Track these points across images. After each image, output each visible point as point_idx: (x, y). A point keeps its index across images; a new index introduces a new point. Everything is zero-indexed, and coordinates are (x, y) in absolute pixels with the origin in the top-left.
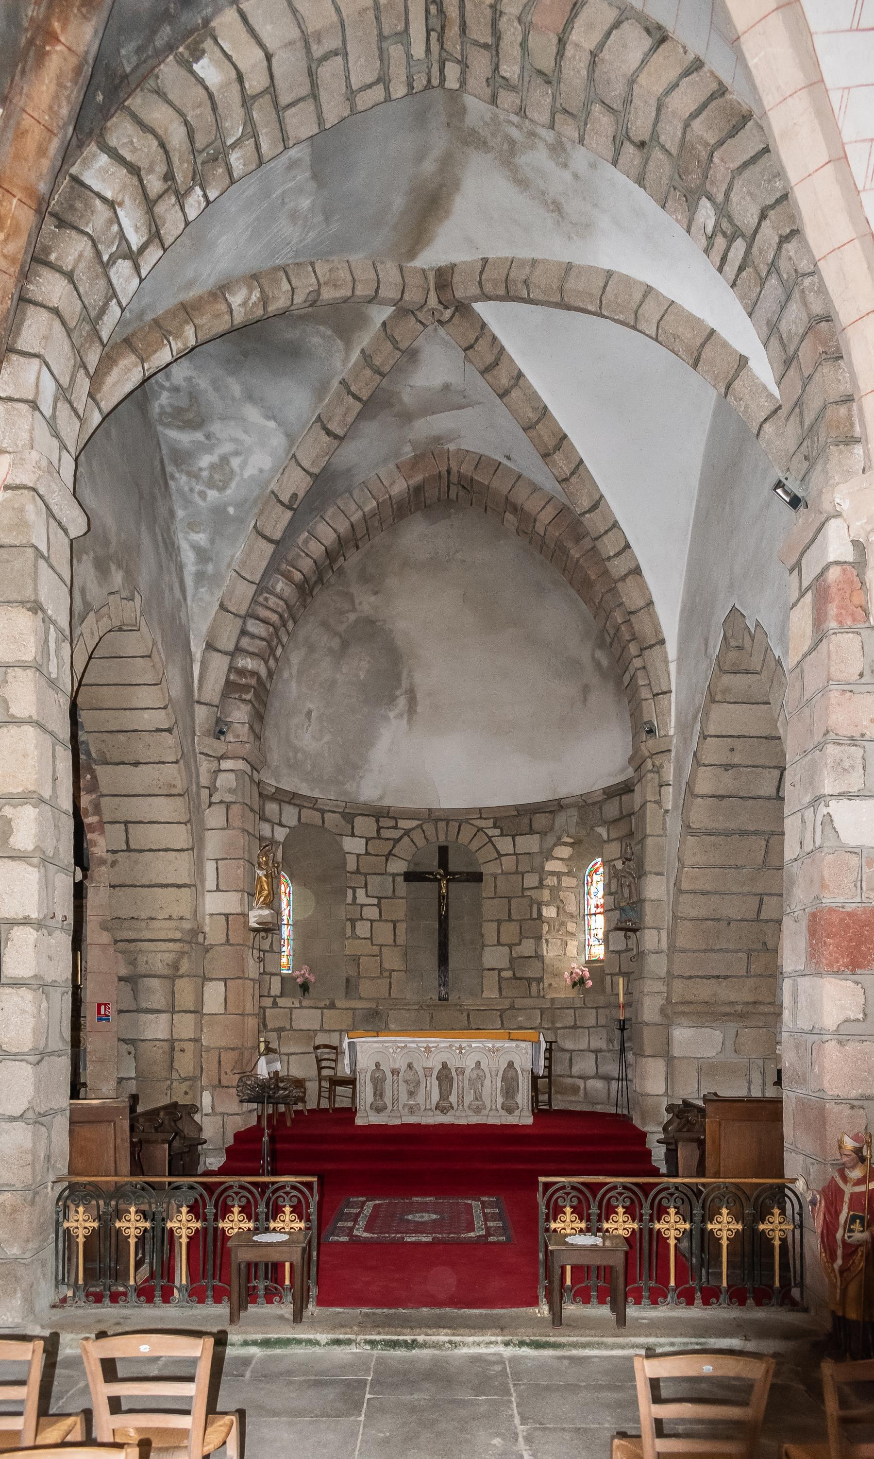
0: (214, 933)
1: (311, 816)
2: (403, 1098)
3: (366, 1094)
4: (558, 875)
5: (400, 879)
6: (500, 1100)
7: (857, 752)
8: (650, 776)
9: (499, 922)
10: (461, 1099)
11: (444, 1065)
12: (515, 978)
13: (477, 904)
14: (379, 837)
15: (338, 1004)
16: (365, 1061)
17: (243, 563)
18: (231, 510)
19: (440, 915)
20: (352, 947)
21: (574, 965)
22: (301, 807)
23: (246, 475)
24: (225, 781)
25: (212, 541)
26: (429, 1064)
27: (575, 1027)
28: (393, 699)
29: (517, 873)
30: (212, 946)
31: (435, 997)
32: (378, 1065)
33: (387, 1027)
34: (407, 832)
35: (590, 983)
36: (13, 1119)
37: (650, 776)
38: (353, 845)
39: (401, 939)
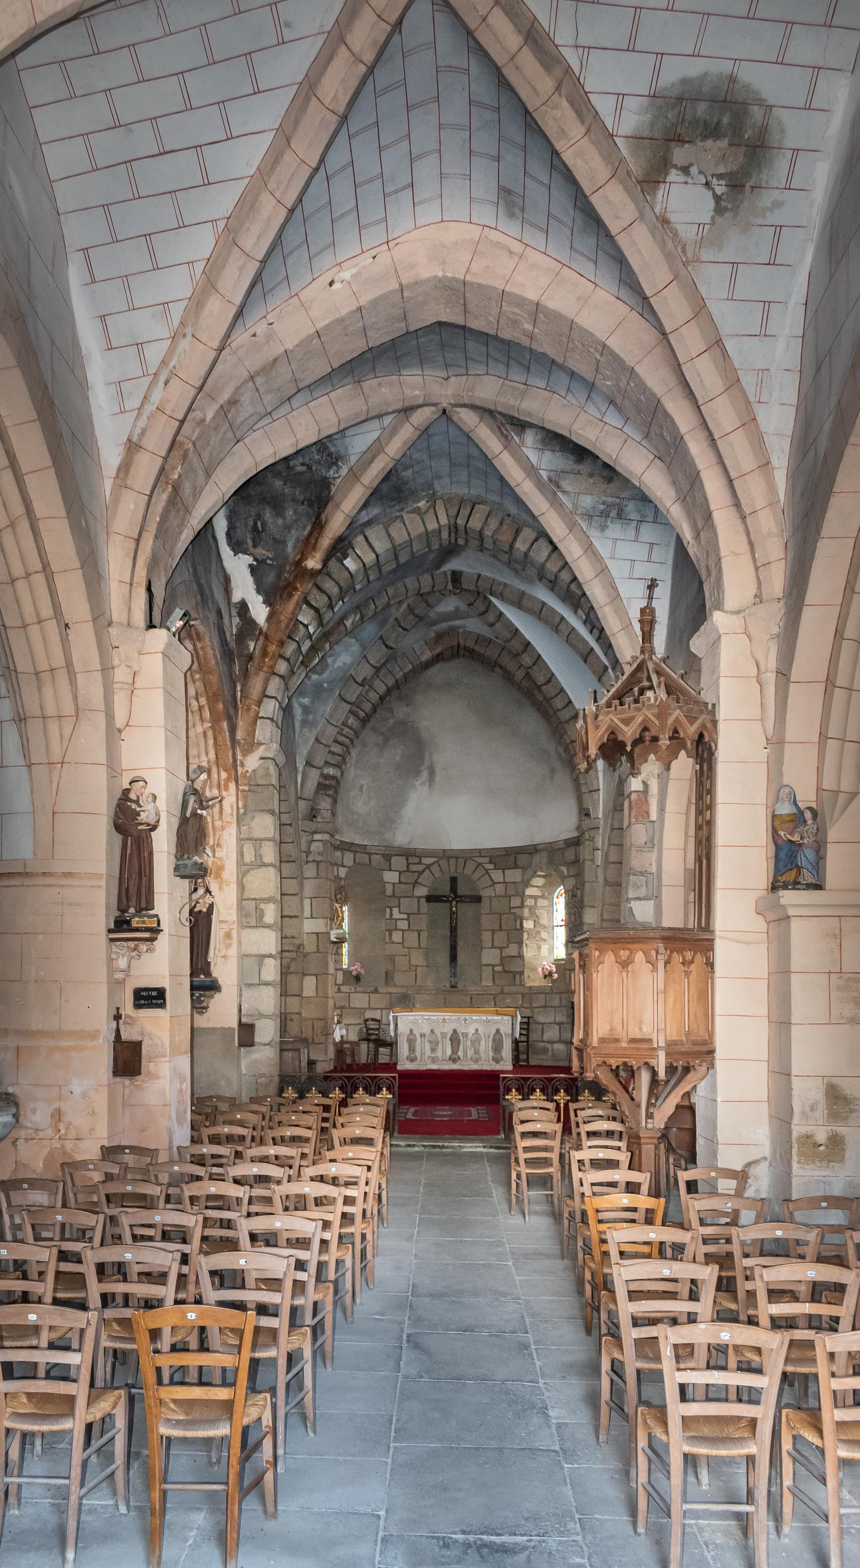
0: (310, 946)
1: (363, 858)
2: (428, 1052)
3: (403, 1050)
4: (535, 898)
5: (423, 900)
6: (491, 1054)
7: (643, 879)
8: (587, 843)
9: (493, 931)
10: (465, 1054)
11: (455, 1031)
12: (505, 971)
13: (478, 919)
14: (408, 870)
15: (381, 990)
16: (403, 1029)
17: (331, 715)
18: (325, 685)
19: (451, 927)
20: (390, 949)
21: (545, 963)
22: (355, 852)
23: (336, 666)
24: (316, 847)
25: (312, 702)
26: (445, 1030)
27: (545, 1007)
28: (418, 773)
29: (506, 896)
30: (308, 954)
31: (448, 985)
32: (411, 1031)
33: (414, 1006)
34: (428, 867)
35: (556, 976)
36: (265, 1045)
37: (587, 843)
38: (391, 877)
39: (424, 944)
